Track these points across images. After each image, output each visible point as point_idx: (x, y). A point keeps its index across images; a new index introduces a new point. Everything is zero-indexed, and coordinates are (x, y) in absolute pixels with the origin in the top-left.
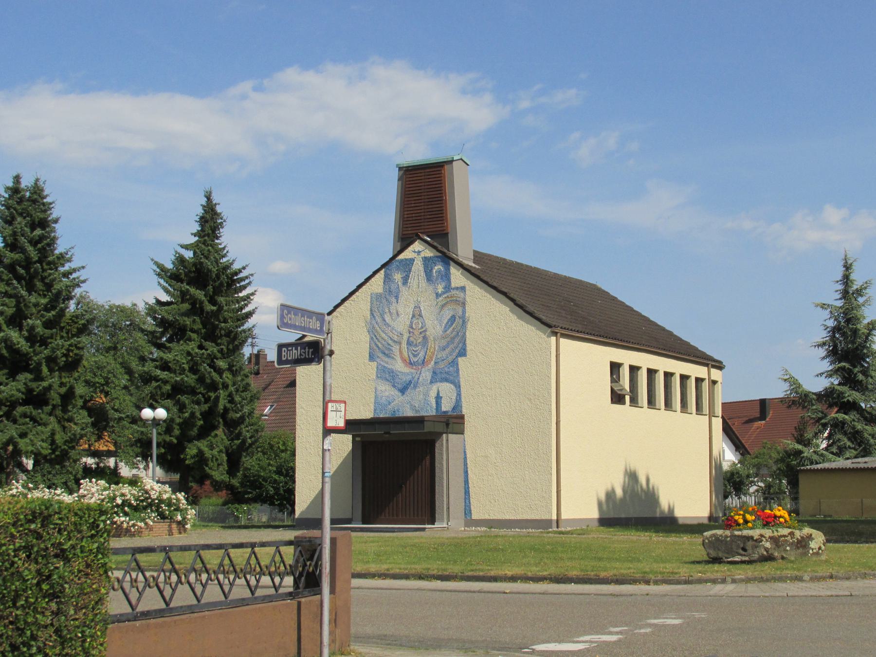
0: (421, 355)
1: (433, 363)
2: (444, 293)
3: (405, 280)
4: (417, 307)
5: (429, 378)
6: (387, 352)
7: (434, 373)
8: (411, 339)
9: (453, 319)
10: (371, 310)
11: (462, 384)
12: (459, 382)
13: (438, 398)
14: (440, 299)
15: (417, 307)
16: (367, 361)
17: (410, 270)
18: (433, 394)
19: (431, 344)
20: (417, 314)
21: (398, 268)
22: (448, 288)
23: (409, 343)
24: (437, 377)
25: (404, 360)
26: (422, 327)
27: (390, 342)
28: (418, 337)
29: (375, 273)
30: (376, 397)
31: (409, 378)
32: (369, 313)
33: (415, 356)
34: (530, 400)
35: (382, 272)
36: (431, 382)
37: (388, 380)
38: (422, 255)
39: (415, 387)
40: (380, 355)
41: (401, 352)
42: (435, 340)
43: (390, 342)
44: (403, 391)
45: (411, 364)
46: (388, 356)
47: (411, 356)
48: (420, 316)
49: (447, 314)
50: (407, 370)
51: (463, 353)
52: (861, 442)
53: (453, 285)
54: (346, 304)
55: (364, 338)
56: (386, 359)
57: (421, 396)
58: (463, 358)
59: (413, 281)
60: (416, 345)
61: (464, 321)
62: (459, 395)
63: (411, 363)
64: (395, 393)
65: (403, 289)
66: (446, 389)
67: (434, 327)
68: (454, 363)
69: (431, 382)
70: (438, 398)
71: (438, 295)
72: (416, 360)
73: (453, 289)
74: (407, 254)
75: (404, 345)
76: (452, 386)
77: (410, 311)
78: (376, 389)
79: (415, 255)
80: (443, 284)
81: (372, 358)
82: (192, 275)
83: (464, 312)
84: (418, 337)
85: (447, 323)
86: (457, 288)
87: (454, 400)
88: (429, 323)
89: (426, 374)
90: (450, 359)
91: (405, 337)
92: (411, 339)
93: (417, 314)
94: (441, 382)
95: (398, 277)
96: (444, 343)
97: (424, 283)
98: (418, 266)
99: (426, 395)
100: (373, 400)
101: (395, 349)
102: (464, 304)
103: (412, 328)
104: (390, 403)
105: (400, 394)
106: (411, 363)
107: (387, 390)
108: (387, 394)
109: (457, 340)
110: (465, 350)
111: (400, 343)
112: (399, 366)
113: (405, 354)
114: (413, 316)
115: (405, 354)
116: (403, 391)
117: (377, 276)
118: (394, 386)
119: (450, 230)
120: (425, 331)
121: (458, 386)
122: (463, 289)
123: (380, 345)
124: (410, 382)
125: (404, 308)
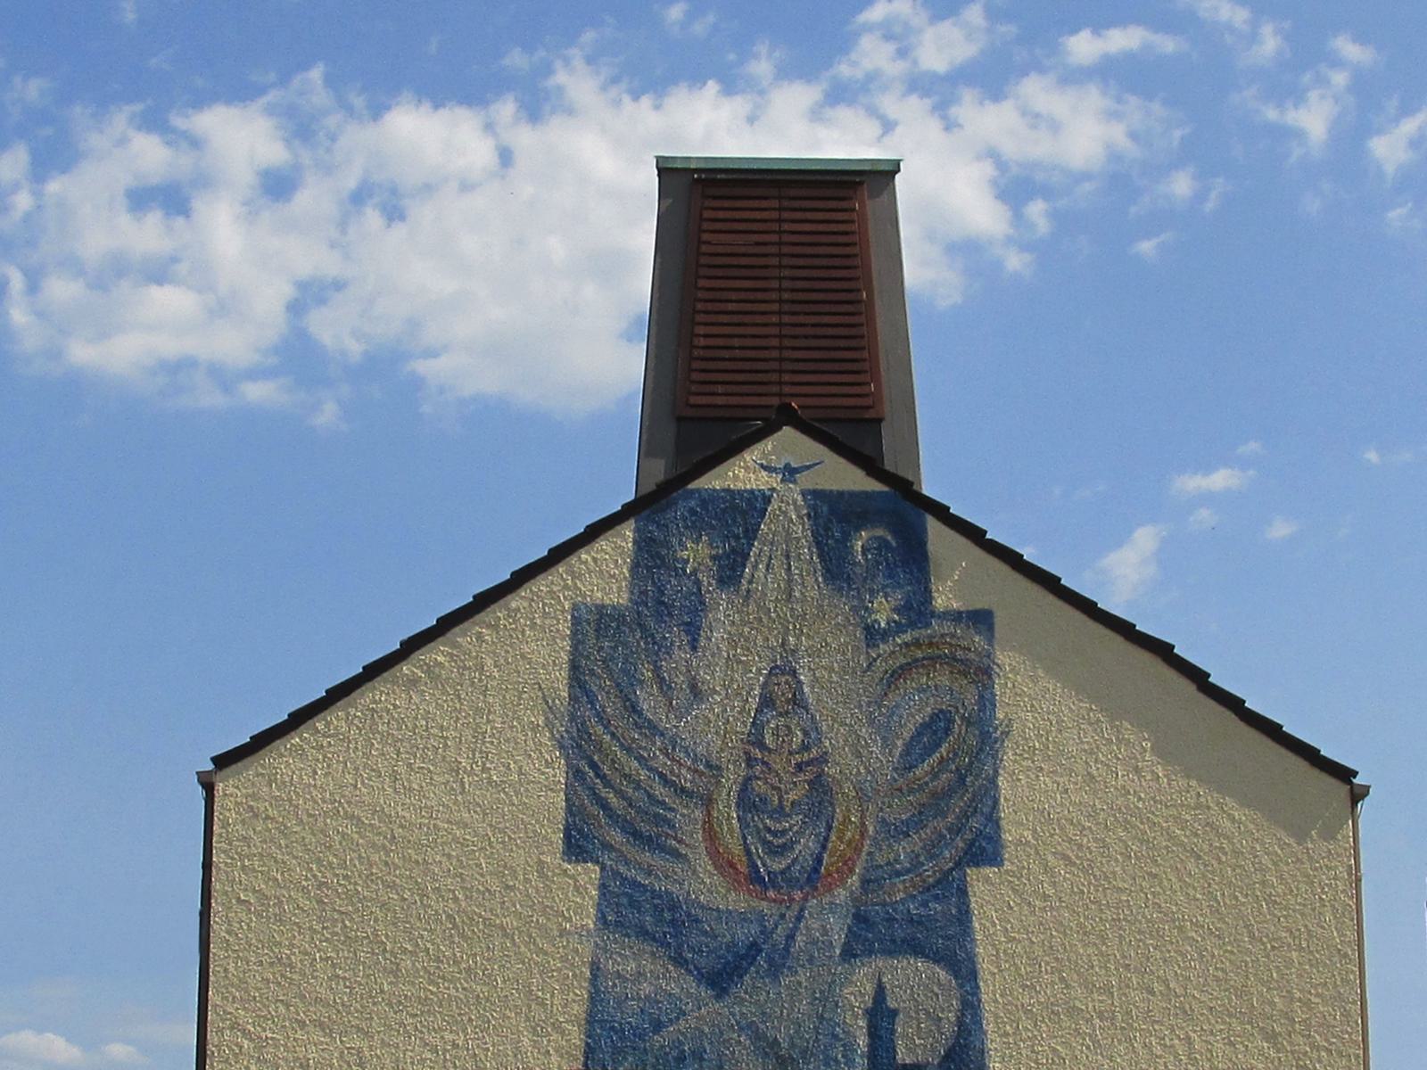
0: (806, 846)
1: (854, 881)
2: (899, 628)
3: (730, 570)
4: (784, 669)
5: (838, 938)
6: (645, 828)
7: (861, 919)
8: (759, 786)
9: (936, 728)
10: (574, 667)
11: (985, 966)
12: (971, 959)
13: (880, 1016)
15: (784, 669)
16: (553, 856)
17: (751, 533)
18: (857, 989)
19: (845, 810)
20: (785, 694)
21: (697, 525)
22: (917, 610)
23: (747, 802)
24: (869, 934)
25: (724, 864)
26: (805, 747)
27: (659, 790)
28: (783, 788)
29: (594, 532)
30: (595, 998)
31: (744, 934)
33: (776, 851)
34: (1271, 1037)
35: (628, 531)
36: (849, 954)
37: (643, 933)
38: (807, 481)
39: (775, 970)
40: (616, 837)
41: (711, 835)
42: (861, 796)
43: (659, 790)
44: (720, 979)
45: (756, 880)
46: (650, 843)
47: (758, 849)
48: (798, 701)
49: (913, 707)
50: (738, 901)
51: (985, 850)
52: (801, 770)
54: (464, 636)
55: (543, 781)
56: (646, 857)
57: (804, 1006)
58: (990, 871)
59: (762, 574)
60: (780, 813)
61: (985, 737)
62: (970, 1006)
63: (755, 877)
64: (679, 985)
66: (912, 979)
67: (857, 742)
68: (952, 889)
69: (849, 954)
70: (880, 1016)
71: (872, 635)
72: (778, 865)
74: (743, 473)
75: (727, 812)
76: (942, 974)
78: (595, 968)
79: (774, 481)
80: (898, 597)
81: (577, 845)
82: (876, 626)
83: (986, 701)
84: (783, 788)
85: (919, 734)
86: (957, 617)
87: (949, 1028)
88: (833, 740)
89: (828, 920)
90: (929, 871)
91: (731, 778)
92: (759, 786)
93: (785, 694)
94: (890, 953)
95: (695, 553)
96: (900, 811)
97: (812, 586)
100: (579, 1010)
101: (687, 818)
102: (982, 674)
103: (761, 745)
104: (658, 1026)
105: (705, 993)
106: (755, 877)
107: (648, 975)
109: (958, 804)
111: (708, 802)
112: (703, 884)
113: (732, 843)
114: (767, 702)
115: (732, 843)
116: (720, 979)
117: (603, 544)
118: (679, 961)
119: (887, 410)
120: (823, 759)
121: (964, 971)
122: (981, 619)
123: (612, 799)
124: (754, 948)
125: (727, 662)
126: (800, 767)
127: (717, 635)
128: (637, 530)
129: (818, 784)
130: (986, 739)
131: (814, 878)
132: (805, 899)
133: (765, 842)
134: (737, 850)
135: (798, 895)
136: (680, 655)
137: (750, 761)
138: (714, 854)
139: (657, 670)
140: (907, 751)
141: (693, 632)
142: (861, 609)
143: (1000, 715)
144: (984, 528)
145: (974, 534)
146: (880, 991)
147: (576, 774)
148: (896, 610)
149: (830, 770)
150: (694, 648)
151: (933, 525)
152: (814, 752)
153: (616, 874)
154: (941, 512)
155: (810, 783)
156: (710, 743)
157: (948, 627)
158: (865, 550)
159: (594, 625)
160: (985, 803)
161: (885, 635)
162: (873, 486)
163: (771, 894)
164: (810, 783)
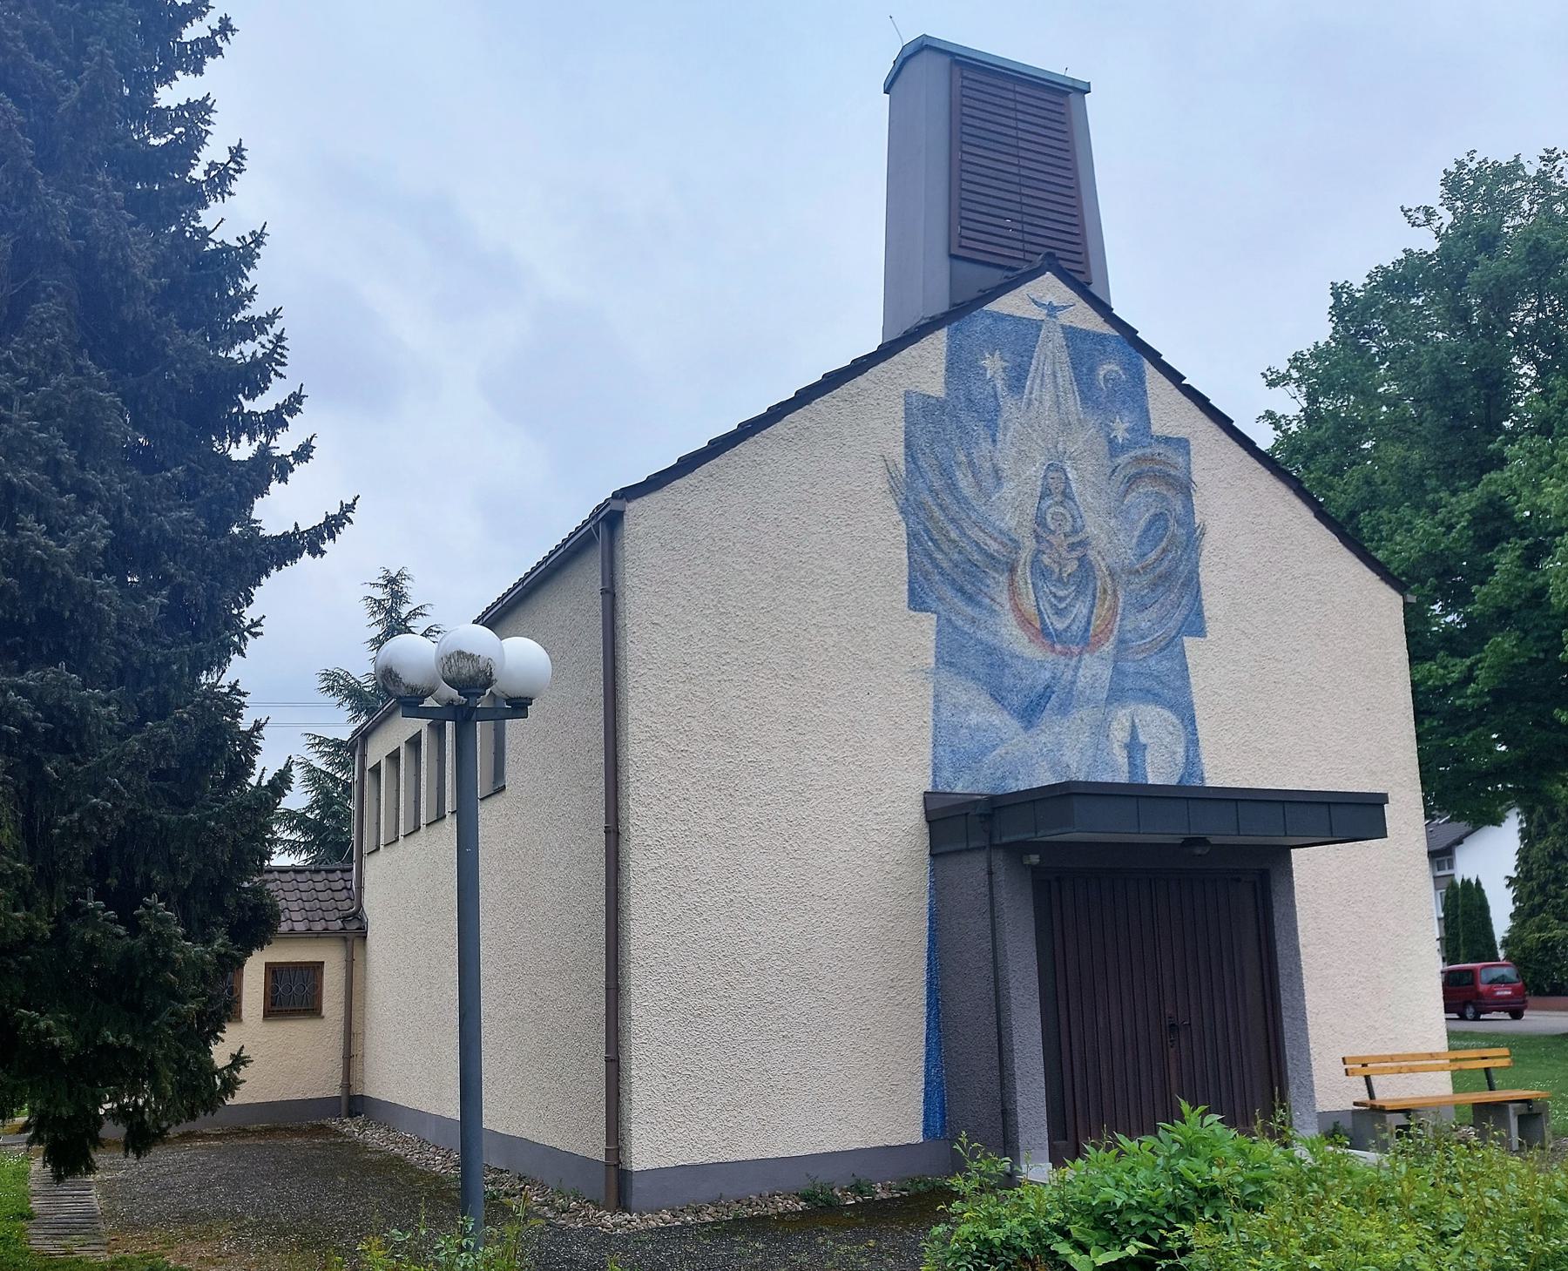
3: (1017, 379)
11: (1200, 714)
12: (1190, 706)
13: (1134, 747)
14: (1123, 459)
18: (1120, 734)
20: (1056, 489)
25: (1025, 622)
26: (1075, 531)
32: (901, 449)
33: (1059, 613)
38: (1065, 318)
39: (1064, 709)
40: (948, 592)
44: (1030, 712)
45: (1045, 634)
46: (971, 599)
48: (1067, 495)
51: (1195, 624)
53: (1156, 428)
55: (886, 539)
56: (969, 610)
61: (1190, 534)
62: (1193, 742)
63: (1044, 632)
65: (1008, 403)
68: (1170, 646)
70: (1134, 747)
71: (1114, 448)
72: (1060, 626)
73: (1159, 440)
76: (1174, 719)
77: (1034, 471)
81: (917, 602)
83: (1190, 511)
87: (1181, 750)
88: (1094, 527)
91: (1025, 555)
93: (1056, 489)
95: (993, 365)
97: (1073, 404)
98: (1050, 354)
99: (1101, 729)
100: (928, 734)
102: (1185, 488)
105: (1015, 724)
106: (1044, 632)
107: (984, 715)
108: (974, 718)
110: (1200, 613)
115: (1028, 603)
116: (1030, 712)
117: (926, 342)
121: (1188, 720)
126: (1072, 547)
127: (1007, 438)
128: (950, 337)
129: (1082, 560)
130: (1192, 540)
131: (1087, 640)
132: (1081, 653)
133: (1053, 606)
134: (1034, 610)
135: (1075, 649)
136: (986, 446)
137: (1037, 537)
138: (1016, 608)
139: (968, 455)
140: (1140, 543)
141: (992, 425)
142: (1105, 428)
143: (1197, 521)
144: (244, 1014)
145: (1175, 377)
146: (1133, 725)
147: (912, 536)
148: (1126, 430)
149: (1092, 554)
150: (994, 441)
151: (1154, 381)
152: (1081, 536)
153: (949, 621)
154: (1155, 357)
155: (1078, 559)
156: (1009, 521)
157: (1160, 449)
158: (1106, 380)
159: (921, 411)
160: (1192, 584)
161: (1124, 448)
162: (1107, 329)
163: (1058, 647)
164: (1078, 559)
